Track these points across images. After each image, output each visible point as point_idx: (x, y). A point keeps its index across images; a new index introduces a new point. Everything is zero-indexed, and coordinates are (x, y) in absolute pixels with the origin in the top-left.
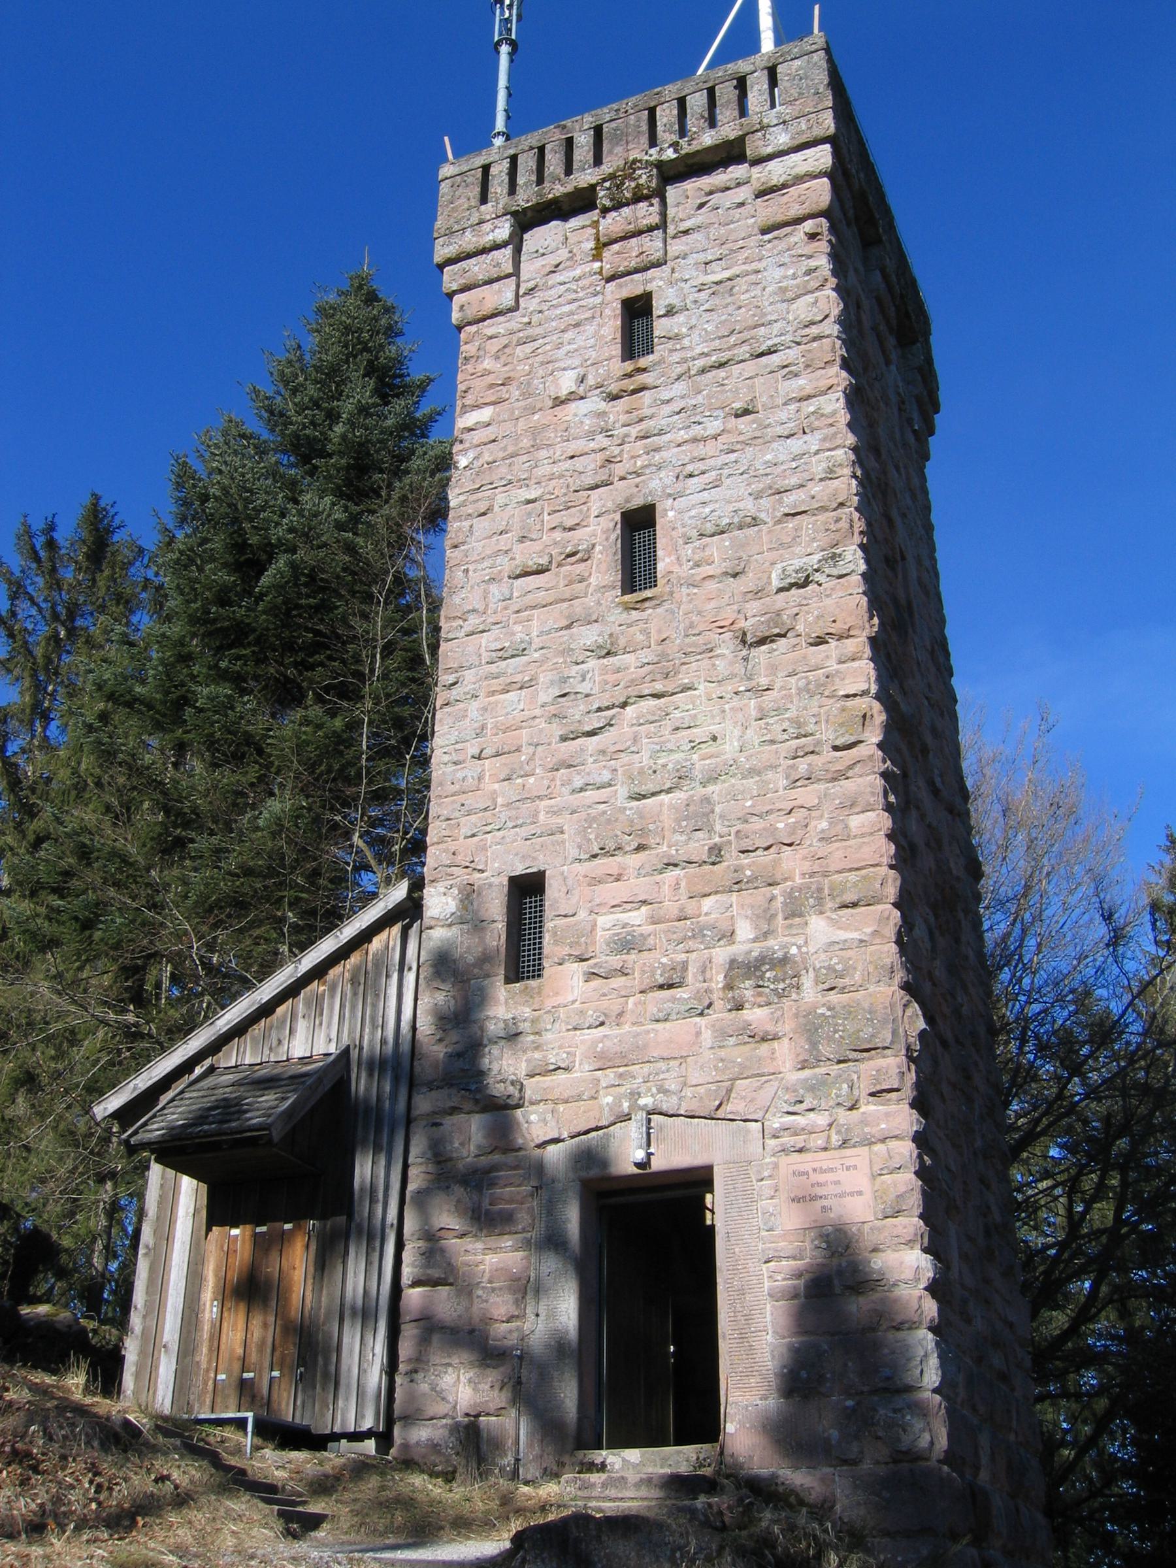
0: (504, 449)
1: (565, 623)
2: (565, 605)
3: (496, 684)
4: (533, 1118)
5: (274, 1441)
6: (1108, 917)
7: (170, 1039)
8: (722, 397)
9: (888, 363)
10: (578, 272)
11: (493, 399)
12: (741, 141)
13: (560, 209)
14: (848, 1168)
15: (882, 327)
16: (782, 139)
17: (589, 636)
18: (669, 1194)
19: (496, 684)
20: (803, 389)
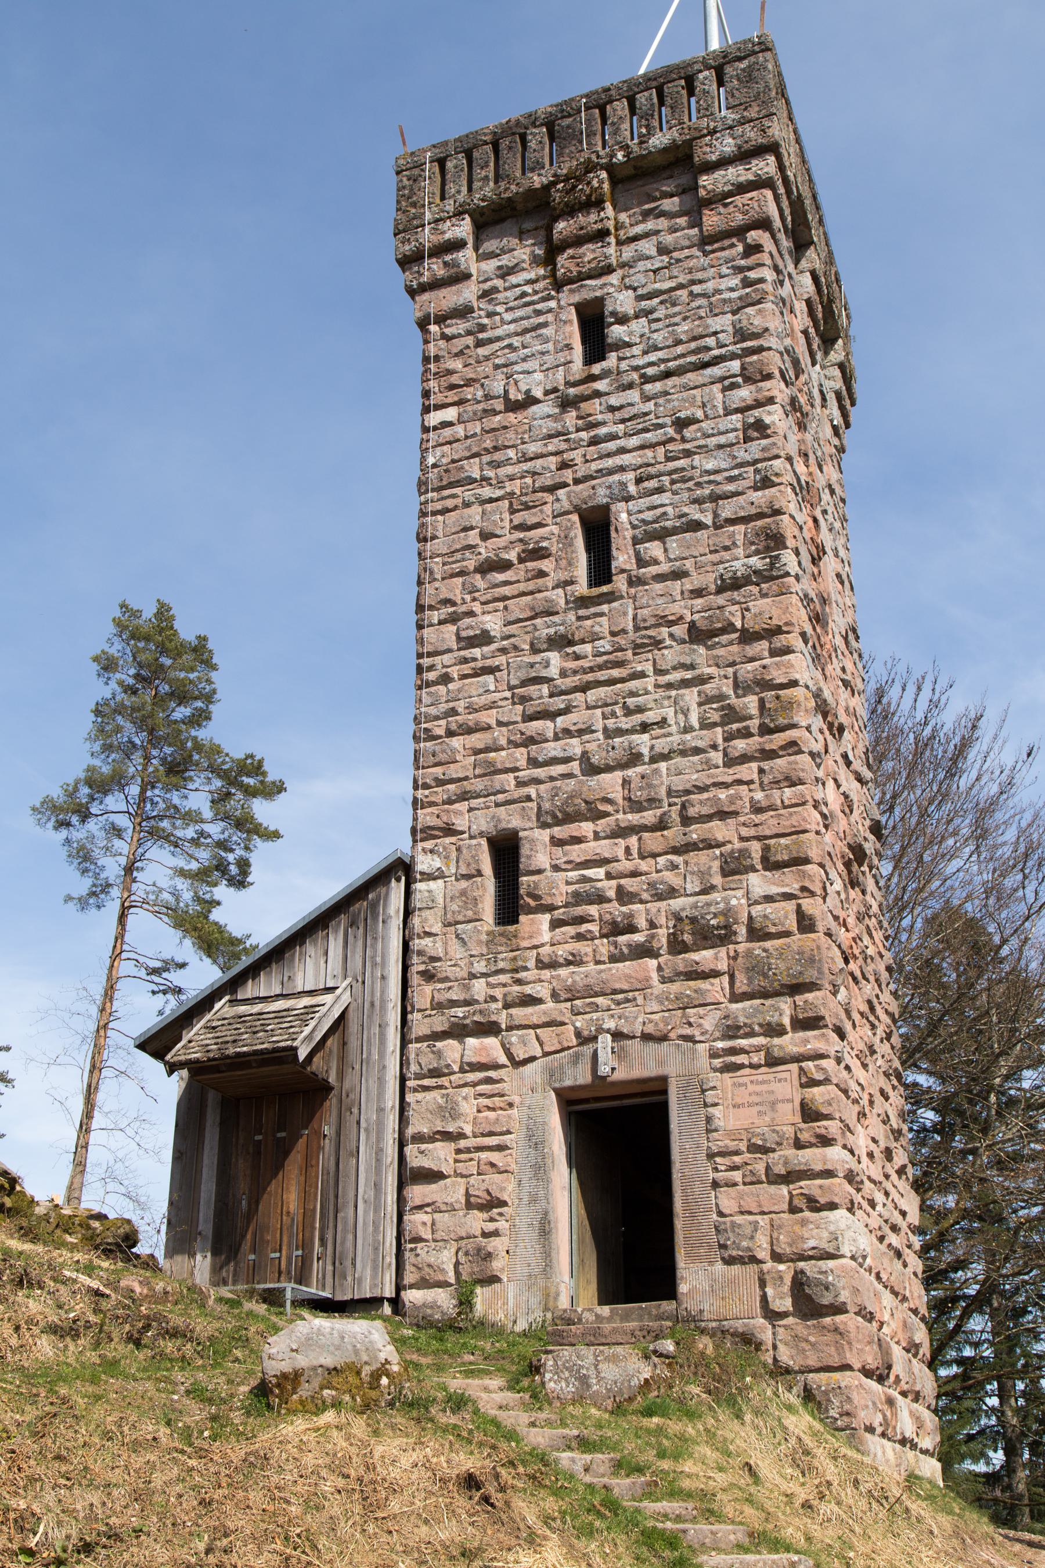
0: (469, 448)
1: (529, 614)
2: (529, 598)
3: (466, 669)
4: (514, 1039)
5: (412, 1168)
6: (974, 727)
7: (493, 817)
8: (669, 406)
9: (814, 364)
10: (532, 275)
11: (456, 399)
12: (689, 144)
13: (514, 209)
14: (780, 1081)
15: (812, 330)
16: (727, 145)
17: (545, 629)
18: (627, 1102)
19: (466, 669)
20: (744, 400)
